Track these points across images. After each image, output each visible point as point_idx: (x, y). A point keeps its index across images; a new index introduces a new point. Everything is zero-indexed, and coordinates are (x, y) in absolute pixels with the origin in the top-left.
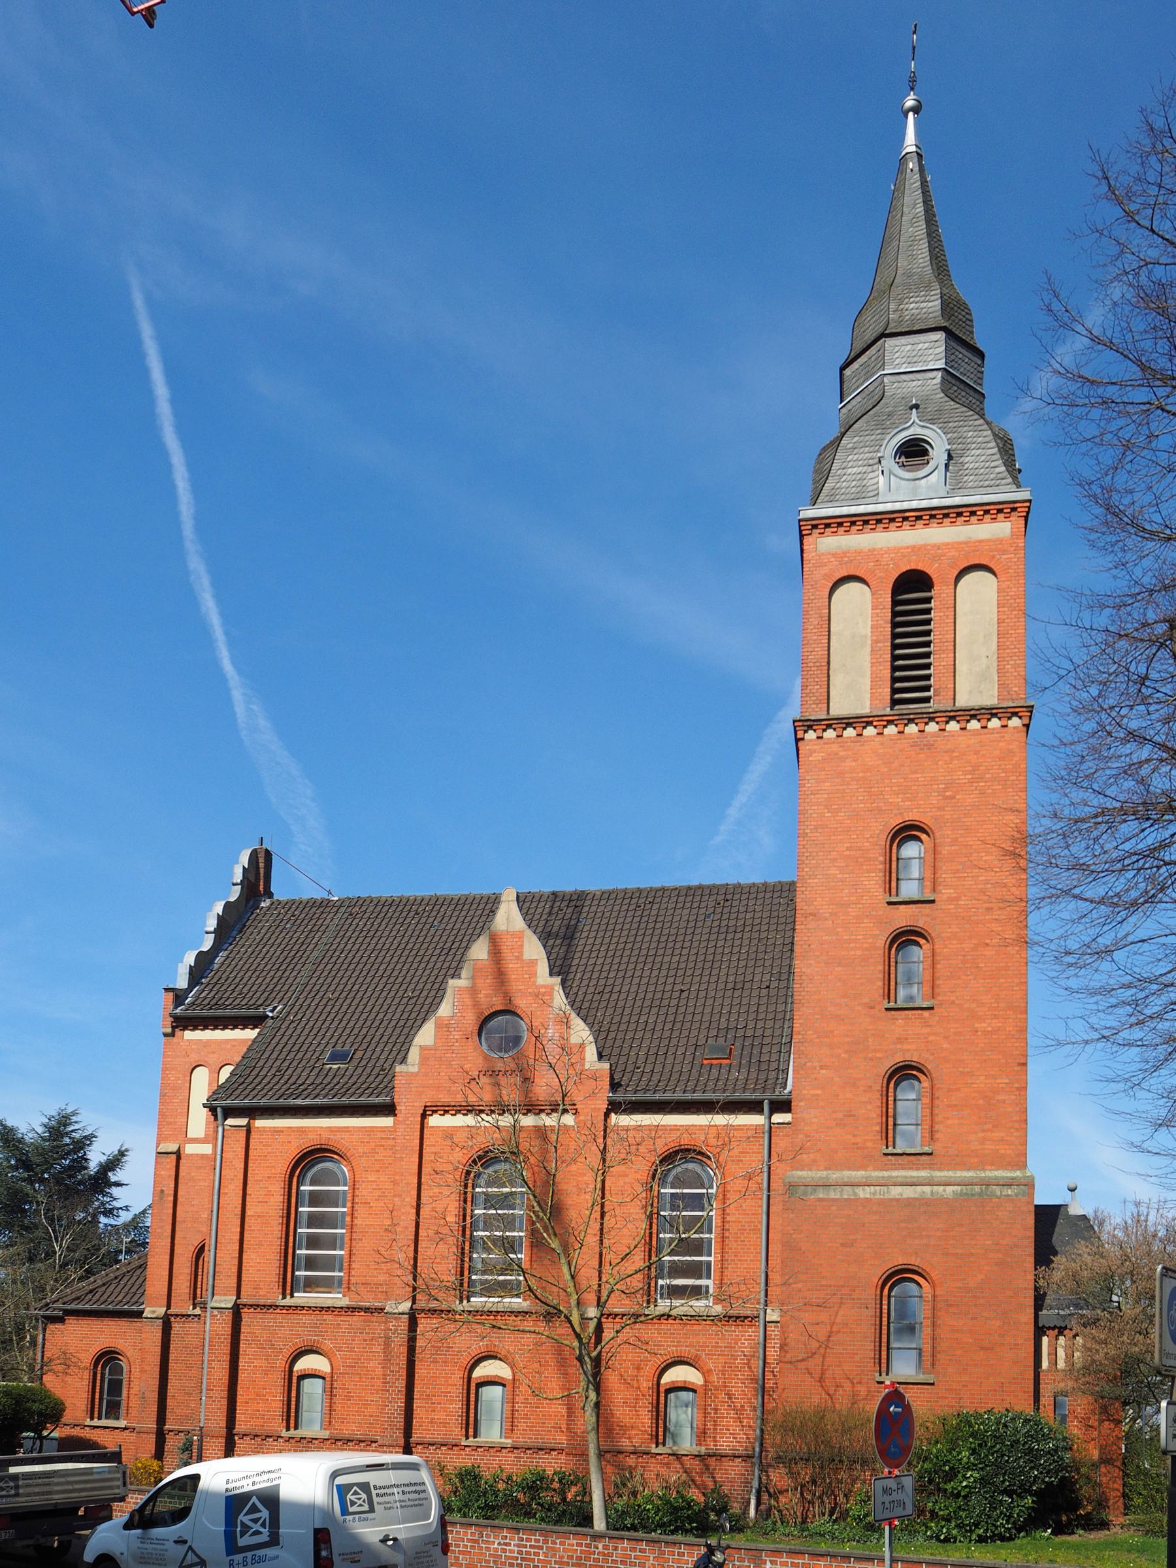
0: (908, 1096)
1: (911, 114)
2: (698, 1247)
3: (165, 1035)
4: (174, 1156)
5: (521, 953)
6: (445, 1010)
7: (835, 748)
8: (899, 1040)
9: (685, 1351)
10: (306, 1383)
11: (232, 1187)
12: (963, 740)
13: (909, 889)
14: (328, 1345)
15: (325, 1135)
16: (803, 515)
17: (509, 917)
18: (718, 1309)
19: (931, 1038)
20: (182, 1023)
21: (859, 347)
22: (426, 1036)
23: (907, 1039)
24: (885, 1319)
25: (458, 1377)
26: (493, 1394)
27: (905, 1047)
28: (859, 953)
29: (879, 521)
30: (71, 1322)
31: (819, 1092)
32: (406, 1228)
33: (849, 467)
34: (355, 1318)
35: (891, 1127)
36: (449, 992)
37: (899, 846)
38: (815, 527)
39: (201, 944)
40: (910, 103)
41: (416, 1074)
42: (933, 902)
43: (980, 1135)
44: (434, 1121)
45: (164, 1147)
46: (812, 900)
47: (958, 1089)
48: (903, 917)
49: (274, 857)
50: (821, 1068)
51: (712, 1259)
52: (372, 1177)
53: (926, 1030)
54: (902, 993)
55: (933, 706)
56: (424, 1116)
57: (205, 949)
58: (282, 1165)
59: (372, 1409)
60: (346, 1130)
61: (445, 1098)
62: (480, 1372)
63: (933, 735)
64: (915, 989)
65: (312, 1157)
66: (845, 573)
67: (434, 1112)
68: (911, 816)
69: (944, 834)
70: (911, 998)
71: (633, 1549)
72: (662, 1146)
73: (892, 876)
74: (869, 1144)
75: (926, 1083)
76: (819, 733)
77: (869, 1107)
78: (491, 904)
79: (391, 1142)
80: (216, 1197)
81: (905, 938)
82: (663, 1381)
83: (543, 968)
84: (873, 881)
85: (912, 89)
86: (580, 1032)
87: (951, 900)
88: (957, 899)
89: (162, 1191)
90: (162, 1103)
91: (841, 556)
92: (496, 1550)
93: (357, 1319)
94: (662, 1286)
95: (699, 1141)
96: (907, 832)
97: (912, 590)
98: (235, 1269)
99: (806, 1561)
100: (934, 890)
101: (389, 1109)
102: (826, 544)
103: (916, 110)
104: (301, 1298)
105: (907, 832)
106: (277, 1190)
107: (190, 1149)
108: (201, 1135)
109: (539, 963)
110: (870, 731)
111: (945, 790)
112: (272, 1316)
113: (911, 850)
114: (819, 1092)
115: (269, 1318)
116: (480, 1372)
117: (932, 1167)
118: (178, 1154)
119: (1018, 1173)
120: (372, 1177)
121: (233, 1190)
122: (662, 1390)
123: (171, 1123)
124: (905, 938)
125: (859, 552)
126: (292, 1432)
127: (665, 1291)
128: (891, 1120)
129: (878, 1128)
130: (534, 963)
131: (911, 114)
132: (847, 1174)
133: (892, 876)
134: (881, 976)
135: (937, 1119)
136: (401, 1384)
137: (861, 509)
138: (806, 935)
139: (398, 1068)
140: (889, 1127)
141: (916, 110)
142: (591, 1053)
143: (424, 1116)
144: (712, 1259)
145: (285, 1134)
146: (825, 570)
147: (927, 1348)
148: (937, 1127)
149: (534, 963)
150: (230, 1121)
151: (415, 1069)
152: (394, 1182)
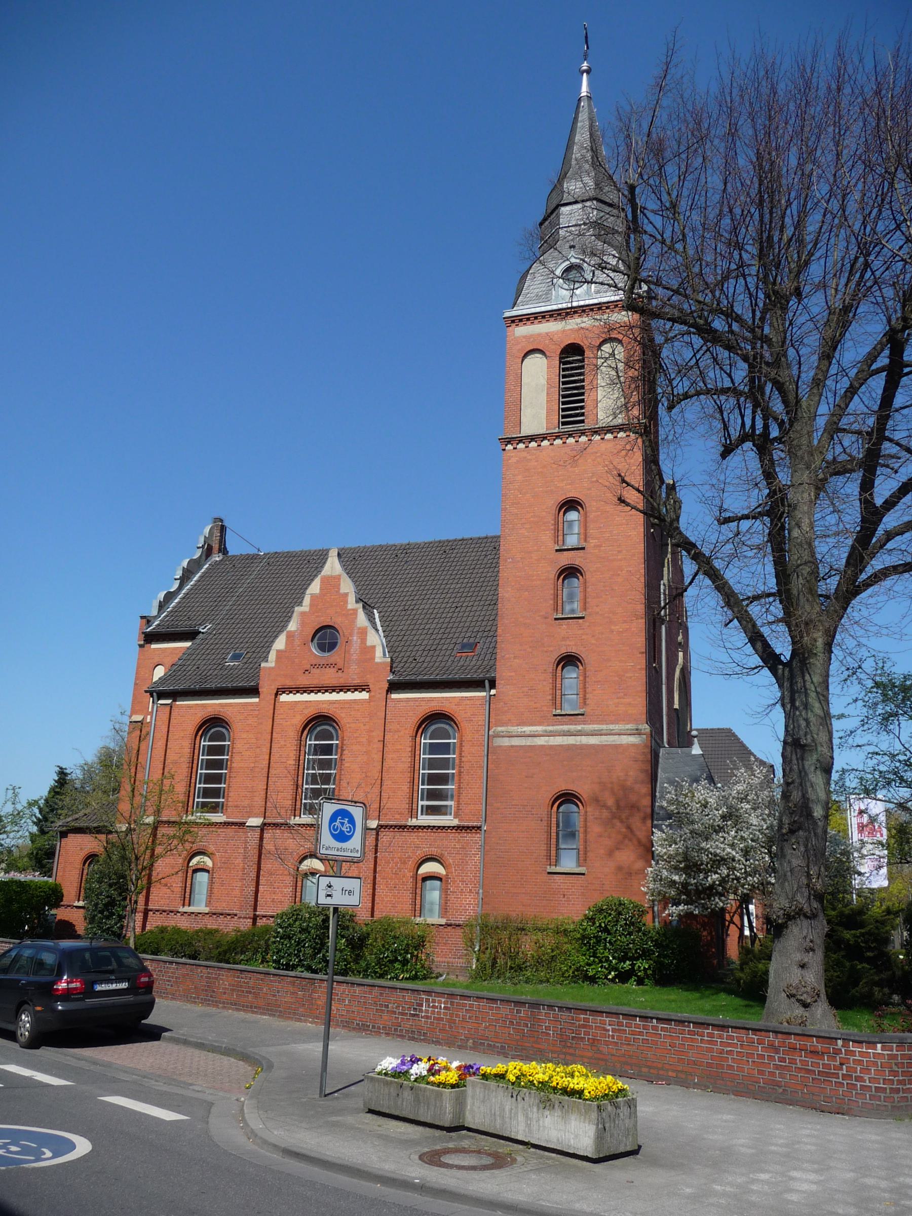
0: (571, 675)
1: (585, 74)
3: (141, 646)
5: (339, 589)
6: (292, 626)
7: (524, 454)
8: (564, 639)
9: (434, 851)
10: (199, 874)
11: (160, 743)
12: (604, 446)
13: (572, 541)
14: (212, 848)
15: (218, 709)
16: (507, 314)
17: (333, 566)
18: (456, 822)
19: (583, 637)
20: (150, 638)
21: (549, 211)
22: (280, 643)
23: (569, 639)
24: (554, 829)
27: (568, 643)
28: (539, 582)
29: (536, 318)
30: (71, 836)
31: (513, 674)
33: (535, 284)
34: (229, 830)
35: (558, 697)
36: (295, 615)
37: (564, 513)
39: (171, 587)
40: (585, 65)
41: (273, 668)
42: (583, 549)
43: (617, 701)
44: (284, 698)
46: (510, 552)
47: (601, 671)
48: (566, 559)
50: (515, 658)
52: (244, 736)
53: (580, 632)
54: (567, 608)
55: (586, 426)
56: (276, 695)
57: (172, 590)
58: (191, 728)
59: (237, 892)
60: (230, 705)
61: (289, 683)
64: (575, 605)
65: (214, 725)
67: (284, 692)
68: (572, 494)
69: (591, 505)
70: (573, 611)
71: (491, 1009)
72: (310, 712)
73: (559, 532)
74: (545, 709)
76: (515, 445)
77: (545, 683)
78: (321, 557)
79: (257, 713)
81: (570, 572)
82: (419, 872)
83: (352, 599)
84: (547, 537)
87: (596, 546)
88: (600, 546)
91: (527, 338)
92: (772, 1074)
93: (230, 831)
94: (422, 806)
96: (571, 504)
97: (572, 354)
99: (710, 1031)
100: (585, 540)
101: (253, 691)
102: (521, 331)
103: (588, 72)
104: (425, 820)
105: (571, 504)
106: (187, 744)
110: (545, 443)
111: (592, 477)
113: (573, 516)
114: (513, 674)
117: (584, 723)
120: (244, 736)
122: (419, 878)
124: (570, 572)
125: (539, 335)
126: (187, 909)
128: (558, 692)
129: (550, 697)
131: (585, 74)
133: (559, 532)
134: (552, 597)
135: (587, 690)
136: (253, 875)
137: (549, 308)
138: (508, 572)
139: (263, 665)
140: (556, 698)
141: (588, 72)
143: (276, 695)
145: (196, 709)
146: (519, 347)
147: (581, 847)
148: (588, 696)
149: (346, 595)
150: (161, 702)
151: (272, 665)
152: (257, 739)
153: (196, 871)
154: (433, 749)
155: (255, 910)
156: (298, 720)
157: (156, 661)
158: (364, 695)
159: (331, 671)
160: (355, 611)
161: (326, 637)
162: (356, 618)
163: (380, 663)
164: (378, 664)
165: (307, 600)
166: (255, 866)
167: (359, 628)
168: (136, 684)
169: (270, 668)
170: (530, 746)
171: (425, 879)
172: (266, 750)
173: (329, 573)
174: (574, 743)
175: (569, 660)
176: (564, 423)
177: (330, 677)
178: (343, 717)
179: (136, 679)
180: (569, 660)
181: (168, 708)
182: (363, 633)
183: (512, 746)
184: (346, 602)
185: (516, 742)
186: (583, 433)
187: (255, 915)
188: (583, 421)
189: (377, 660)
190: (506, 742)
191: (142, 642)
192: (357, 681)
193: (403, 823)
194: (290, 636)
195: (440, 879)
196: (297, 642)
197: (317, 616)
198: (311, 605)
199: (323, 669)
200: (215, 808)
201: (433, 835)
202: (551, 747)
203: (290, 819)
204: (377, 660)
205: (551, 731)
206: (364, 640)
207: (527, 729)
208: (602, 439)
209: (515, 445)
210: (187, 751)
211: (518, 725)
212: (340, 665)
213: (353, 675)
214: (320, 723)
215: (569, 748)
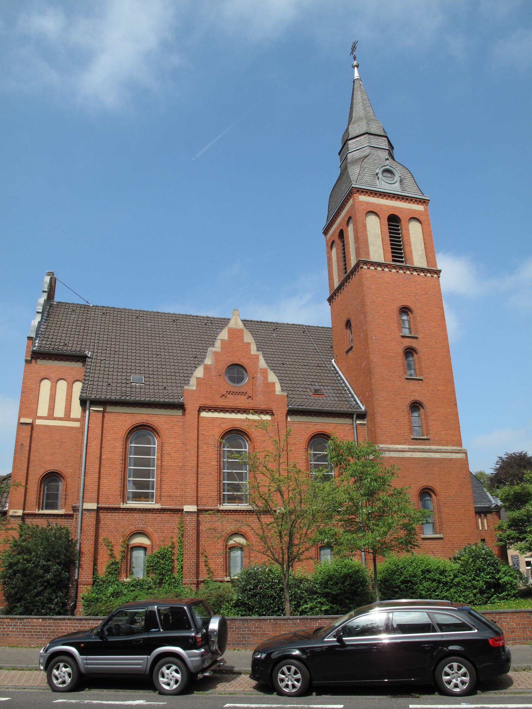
1: (356, 68)
2: (148, 474)
4: (30, 426)
5: (243, 339)
6: (208, 361)
11: (94, 443)
12: (419, 277)
14: (149, 530)
18: (158, 506)
22: (199, 372)
23: (416, 392)
25: (220, 545)
26: (237, 554)
32: (192, 467)
38: (358, 191)
41: (194, 391)
44: (203, 414)
45: (23, 420)
48: (408, 343)
49: (57, 281)
51: (155, 480)
52: (172, 441)
61: (209, 403)
62: (231, 542)
63: (408, 275)
66: (373, 210)
70: (411, 375)
72: (227, 426)
74: (406, 434)
75: (422, 410)
80: (85, 448)
85: (355, 60)
86: (272, 377)
89: (22, 444)
90: (22, 397)
93: (165, 516)
95: (244, 427)
97: (393, 221)
98: (96, 488)
103: (357, 66)
104: (227, 506)
106: (119, 445)
107: (38, 422)
108: (46, 415)
109: (252, 344)
112: (117, 514)
115: (116, 516)
116: (231, 542)
118: (32, 425)
119: (460, 448)
120: (172, 441)
121: (95, 445)
122: (228, 547)
123: (27, 408)
127: (226, 497)
130: (249, 344)
131: (356, 68)
132: (399, 447)
139: (186, 387)
142: (278, 388)
144: (155, 480)
149: (249, 344)
153: (232, 548)
154: (138, 451)
155: (197, 577)
156: (217, 432)
157: (43, 374)
158: (268, 417)
159: (243, 398)
160: (257, 357)
161: (236, 371)
162: (258, 361)
163: (280, 395)
164: (277, 395)
165: (218, 344)
166: (195, 543)
167: (261, 369)
168: (23, 392)
169: (192, 391)
170: (402, 458)
171: (232, 548)
172: (194, 452)
173: (234, 327)
174: (427, 456)
175: (416, 406)
176: (394, 261)
177: (241, 402)
178: (254, 433)
179: (23, 387)
180: (416, 406)
181: (101, 415)
182: (264, 373)
183: (391, 457)
184: (250, 349)
185: (393, 454)
186: (401, 268)
187: (198, 581)
188: (402, 262)
189: (277, 393)
190: (387, 455)
191: (30, 358)
192: (263, 407)
193: (117, 506)
194: (207, 369)
195: (145, 548)
196: (213, 373)
197: (227, 356)
198: (222, 348)
199: (237, 396)
200: (146, 497)
201: (142, 516)
202: (415, 459)
203: (120, 504)
204: (277, 393)
205: (413, 449)
206: (266, 378)
207: (399, 447)
208: (419, 275)
209: (369, 266)
210: (119, 449)
211: (391, 444)
212: (250, 393)
213: (260, 402)
214: (235, 434)
215: (424, 459)
